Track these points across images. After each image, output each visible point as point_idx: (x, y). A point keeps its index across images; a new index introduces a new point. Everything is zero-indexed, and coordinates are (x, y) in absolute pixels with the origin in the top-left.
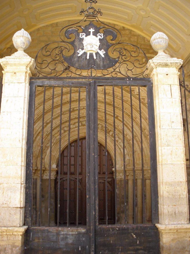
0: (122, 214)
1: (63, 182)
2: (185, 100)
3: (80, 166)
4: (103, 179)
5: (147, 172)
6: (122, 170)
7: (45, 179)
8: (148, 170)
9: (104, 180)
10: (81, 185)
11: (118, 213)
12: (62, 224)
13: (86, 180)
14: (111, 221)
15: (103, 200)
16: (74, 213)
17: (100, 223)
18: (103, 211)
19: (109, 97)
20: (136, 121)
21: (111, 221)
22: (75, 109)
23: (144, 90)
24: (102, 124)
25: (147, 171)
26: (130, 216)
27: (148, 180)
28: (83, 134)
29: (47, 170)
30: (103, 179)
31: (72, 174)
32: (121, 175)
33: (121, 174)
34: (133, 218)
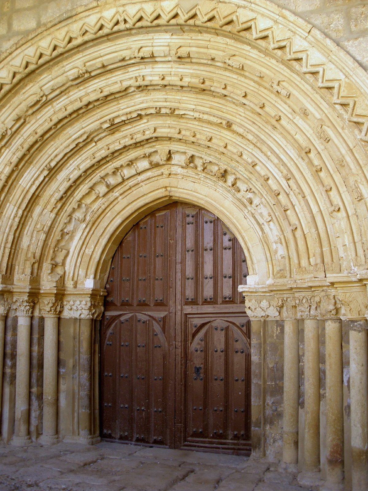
3: (231, 279)
5: (323, 294)
7: (67, 319)
8: (325, 288)
9: (226, 321)
11: (258, 425)
12: (117, 440)
13: (115, 322)
15: (222, 380)
17: (248, 447)
18: (221, 411)
19: (196, 67)
22: (117, 121)
23: (281, 18)
26: (286, 436)
27: (330, 322)
30: (226, 319)
32: (265, 304)
33: (264, 301)
34: (296, 443)
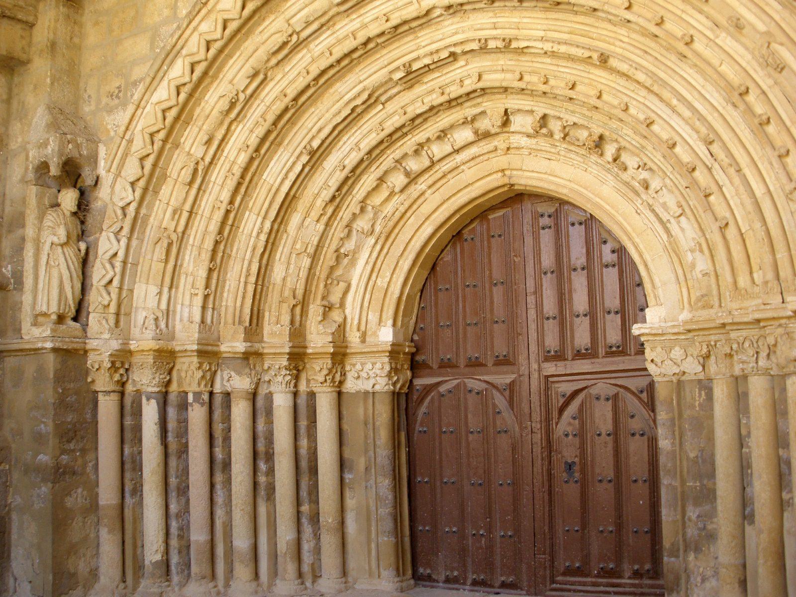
0: (691, 557)
1: (440, 402)
2: (282, 78)
3: (619, 315)
4: (613, 381)
5: (780, 331)
6: (676, 330)
8: (783, 321)
10: (513, 410)
12: (441, 584)
14: (652, 587)
15: (610, 481)
16: (484, 540)
20: (581, 98)
21: (652, 587)
24: (557, 114)
25: (780, 325)
28: (495, 176)
29: (352, 353)
31: (504, 362)
32: (678, 354)
33: (677, 348)
